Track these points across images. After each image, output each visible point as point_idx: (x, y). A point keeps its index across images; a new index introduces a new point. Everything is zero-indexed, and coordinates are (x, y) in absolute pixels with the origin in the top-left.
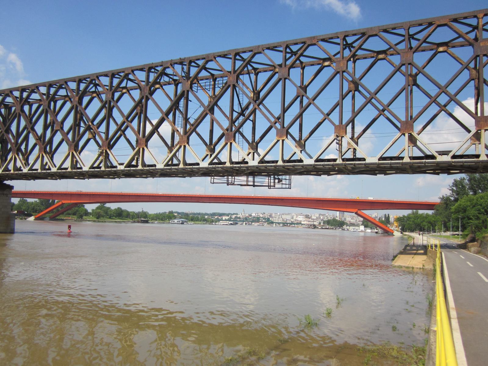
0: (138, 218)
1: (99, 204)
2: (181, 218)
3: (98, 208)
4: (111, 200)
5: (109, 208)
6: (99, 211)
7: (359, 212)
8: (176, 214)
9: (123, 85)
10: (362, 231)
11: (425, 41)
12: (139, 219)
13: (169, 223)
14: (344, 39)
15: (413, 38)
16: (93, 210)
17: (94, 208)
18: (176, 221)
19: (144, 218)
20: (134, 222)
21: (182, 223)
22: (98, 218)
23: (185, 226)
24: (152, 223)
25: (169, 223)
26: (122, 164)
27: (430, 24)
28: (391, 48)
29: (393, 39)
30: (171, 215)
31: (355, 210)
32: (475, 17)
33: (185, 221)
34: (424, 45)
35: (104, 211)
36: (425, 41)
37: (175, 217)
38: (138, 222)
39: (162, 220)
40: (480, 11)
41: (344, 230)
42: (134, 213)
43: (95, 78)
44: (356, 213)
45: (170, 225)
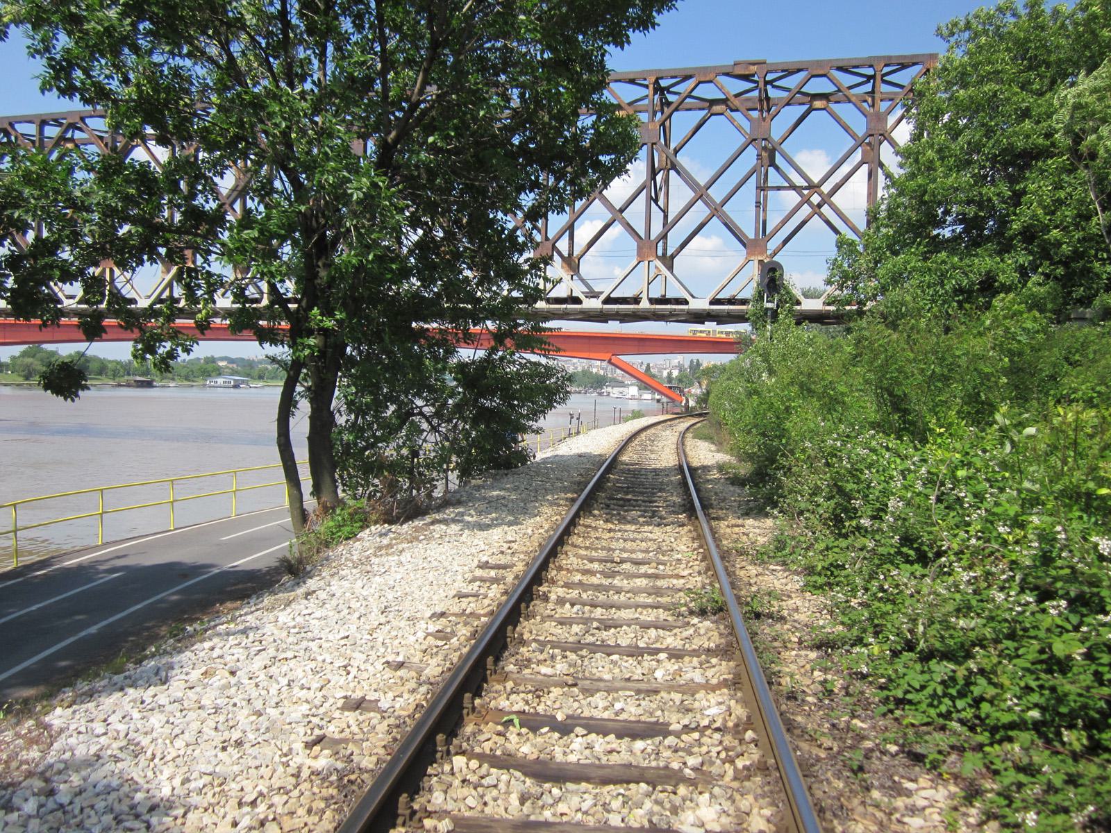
0: (129, 374)
1: (23, 347)
2: (234, 373)
3: (24, 354)
4: (57, 338)
5: (53, 353)
6: (28, 360)
7: (614, 359)
8: (222, 364)
9: (69, 135)
10: (633, 398)
11: (689, 96)
12: (131, 378)
13: (204, 385)
14: (657, 81)
15: (669, 92)
16: (13, 358)
17: (17, 354)
18: (220, 381)
19: (143, 375)
20: (119, 385)
21: (236, 386)
22: (27, 378)
23: (243, 392)
24: (163, 387)
25: (204, 385)
26: (595, 295)
27: (686, 78)
28: (839, 90)
29: (846, 80)
30: (210, 367)
31: (608, 356)
32: (871, 66)
33: (243, 382)
34: (688, 100)
35: (42, 360)
36: (689, 96)
37: (219, 372)
38: (128, 385)
39: (187, 378)
40: (879, 58)
41: (601, 394)
42: (118, 363)
43: (77, 120)
44: (610, 362)
45: (208, 394)
